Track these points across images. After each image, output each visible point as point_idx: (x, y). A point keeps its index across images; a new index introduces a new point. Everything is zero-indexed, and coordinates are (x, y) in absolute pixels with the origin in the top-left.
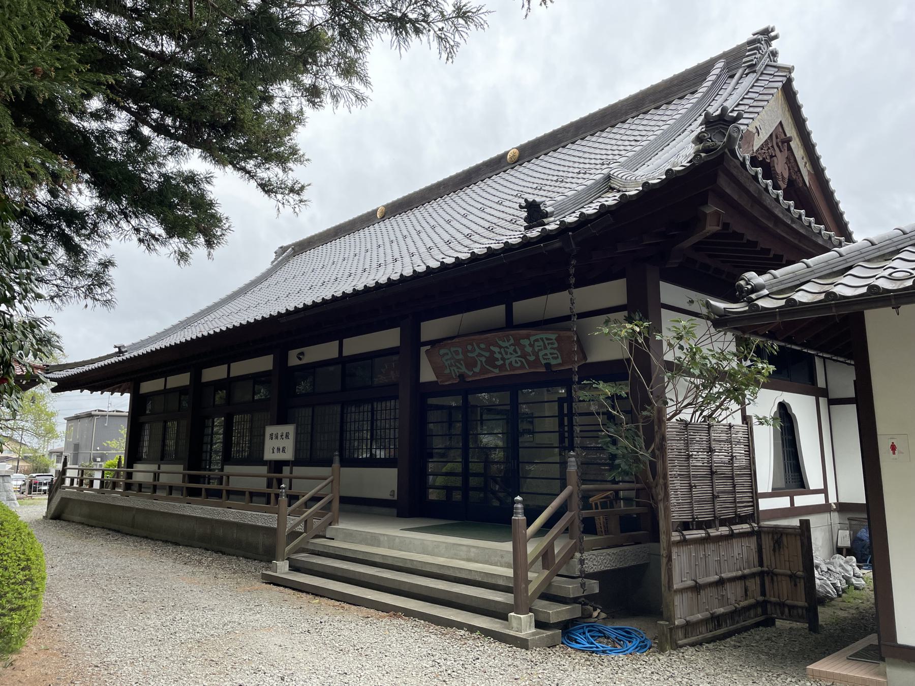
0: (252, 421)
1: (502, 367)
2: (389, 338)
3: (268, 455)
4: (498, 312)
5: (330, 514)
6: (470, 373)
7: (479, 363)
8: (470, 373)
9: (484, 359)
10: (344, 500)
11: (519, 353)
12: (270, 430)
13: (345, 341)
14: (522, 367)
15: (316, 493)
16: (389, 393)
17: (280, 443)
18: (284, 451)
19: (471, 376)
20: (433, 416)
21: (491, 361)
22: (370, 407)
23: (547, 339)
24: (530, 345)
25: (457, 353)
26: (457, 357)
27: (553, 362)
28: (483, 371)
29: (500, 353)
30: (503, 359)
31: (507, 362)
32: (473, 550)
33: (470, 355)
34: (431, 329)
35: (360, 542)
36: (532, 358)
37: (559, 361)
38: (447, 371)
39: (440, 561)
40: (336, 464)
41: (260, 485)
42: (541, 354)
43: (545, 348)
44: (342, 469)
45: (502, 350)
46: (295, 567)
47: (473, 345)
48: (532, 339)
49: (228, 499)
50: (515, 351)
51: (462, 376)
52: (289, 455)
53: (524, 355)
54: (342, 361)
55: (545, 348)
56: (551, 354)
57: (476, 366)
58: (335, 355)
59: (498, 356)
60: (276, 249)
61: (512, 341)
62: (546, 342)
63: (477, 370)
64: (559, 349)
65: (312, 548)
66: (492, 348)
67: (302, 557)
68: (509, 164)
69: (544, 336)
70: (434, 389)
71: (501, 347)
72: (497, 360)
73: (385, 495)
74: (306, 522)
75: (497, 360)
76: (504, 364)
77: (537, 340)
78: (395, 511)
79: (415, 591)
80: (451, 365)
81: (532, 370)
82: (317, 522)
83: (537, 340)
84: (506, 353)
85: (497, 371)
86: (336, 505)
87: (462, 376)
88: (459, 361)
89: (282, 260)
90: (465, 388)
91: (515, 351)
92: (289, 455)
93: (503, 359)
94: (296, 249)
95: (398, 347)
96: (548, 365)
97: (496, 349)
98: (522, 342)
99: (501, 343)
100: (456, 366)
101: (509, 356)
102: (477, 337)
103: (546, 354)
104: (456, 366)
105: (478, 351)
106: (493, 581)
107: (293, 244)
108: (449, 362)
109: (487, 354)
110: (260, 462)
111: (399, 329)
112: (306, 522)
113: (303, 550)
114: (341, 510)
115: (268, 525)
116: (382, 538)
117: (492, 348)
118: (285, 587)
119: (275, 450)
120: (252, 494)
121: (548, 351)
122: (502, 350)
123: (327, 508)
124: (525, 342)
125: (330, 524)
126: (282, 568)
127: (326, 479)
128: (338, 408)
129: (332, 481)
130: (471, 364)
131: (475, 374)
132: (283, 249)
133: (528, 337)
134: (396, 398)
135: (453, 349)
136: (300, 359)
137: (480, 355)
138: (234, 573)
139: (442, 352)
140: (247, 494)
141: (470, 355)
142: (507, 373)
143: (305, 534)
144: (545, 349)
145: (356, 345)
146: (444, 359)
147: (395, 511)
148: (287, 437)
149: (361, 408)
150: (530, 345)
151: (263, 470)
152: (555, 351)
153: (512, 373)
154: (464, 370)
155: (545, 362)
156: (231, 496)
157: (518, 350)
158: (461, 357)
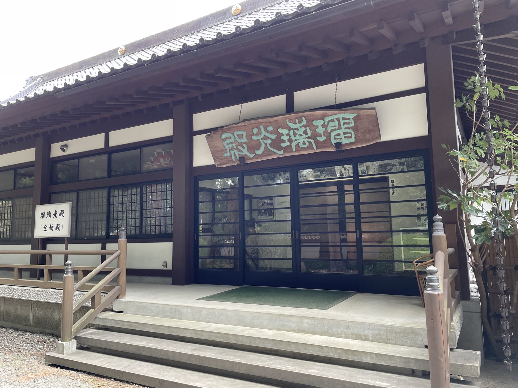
0: (13, 206)
1: (286, 149)
2: (163, 128)
3: (39, 233)
4: (280, 100)
5: (117, 288)
6: (252, 156)
7: (263, 146)
8: (252, 156)
9: (269, 142)
10: (132, 273)
11: (309, 134)
12: (40, 209)
13: (111, 133)
14: (310, 147)
15: (104, 268)
16: (163, 177)
17: (53, 221)
18: (57, 228)
19: (251, 157)
20: (202, 196)
21: (277, 143)
22: (139, 190)
23: (344, 119)
24: (323, 126)
25: (240, 136)
26: (240, 141)
27: (345, 141)
28: (267, 152)
29: (288, 135)
30: (290, 141)
31: (294, 143)
32: (306, 321)
33: (254, 138)
34: (203, 120)
35: (157, 315)
36: (322, 139)
37: (353, 140)
38: (227, 155)
39: (355, 345)
40: (123, 240)
41: (25, 261)
42: (333, 134)
43: (340, 128)
44: (128, 244)
45: (291, 132)
46: (84, 346)
47: (259, 128)
48: (327, 119)
49: (51, 278)
50: (305, 132)
51: (242, 159)
52: (64, 232)
53: (314, 136)
54: (108, 151)
55: (340, 128)
56: (344, 133)
57: (259, 149)
58: (102, 145)
59: (285, 138)
60: (28, 77)
61: (304, 122)
62: (342, 122)
63: (259, 152)
64: (355, 129)
65: (101, 323)
66: (280, 130)
67: (90, 334)
68: (233, 16)
69: (340, 116)
70: (210, 172)
71: (290, 129)
72: (284, 141)
73: (157, 266)
74: (93, 298)
75: (284, 141)
76: (291, 146)
77: (332, 121)
78: (170, 280)
79: (255, 373)
80: (233, 149)
81: (320, 150)
82: (105, 297)
83: (332, 121)
84: (295, 135)
85: (281, 153)
86: (123, 278)
87: (242, 159)
88: (241, 145)
89: (33, 86)
90: (243, 170)
91: (305, 132)
92: (64, 232)
93: (290, 141)
94: (45, 78)
95: (172, 136)
96: (338, 145)
97: (285, 132)
98: (315, 123)
99: (291, 125)
100: (237, 149)
101: (298, 137)
102: (265, 120)
103: (339, 134)
104: (237, 149)
105: (264, 133)
106: (351, 358)
107: (42, 75)
108: (230, 146)
109: (273, 137)
110: (28, 239)
111: (172, 120)
112: (93, 298)
113: (90, 326)
114: (128, 281)
115: (42, 300)
116: (184, 310)
117: (280, 130)
118: (78, 371)
119: (48, 228)
120: (21, 270)
121: (341, 132)
122: (291, 132)
123: (115, 280)
124: (319, 123)
125: (117, 298)
126: (69, 350)
127: (113, 254)
128: (105, 193)
129: (118, 256)
130: (253, 147)
131: (257, 156)
132: (33, 79)
133: (323, 118)
134: (170, 180)
135: (236, 133)
136: (64, 151)
137: (266, 138)
138: (9, 353)
139: (224, 136)
140: (16, 271)
141: (254, 138)
142: (292, 154)
143: (92, 311)
144: (341, 131)
145: (120, 137)
146: (225, 143)
147: (170, 280)
148: (61, 214)
149: (129, 192)
150: (323, 126)
151: (27, 247)
152: (351, 131)
153: (297, 154)
154: (245, 152)
155: (337, 141)
156: (54, 275)
157: (308, 130)
158: (245, 140)
